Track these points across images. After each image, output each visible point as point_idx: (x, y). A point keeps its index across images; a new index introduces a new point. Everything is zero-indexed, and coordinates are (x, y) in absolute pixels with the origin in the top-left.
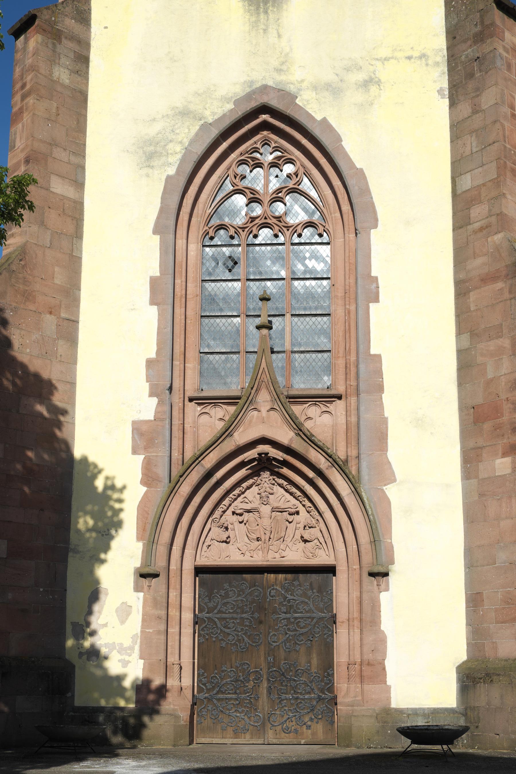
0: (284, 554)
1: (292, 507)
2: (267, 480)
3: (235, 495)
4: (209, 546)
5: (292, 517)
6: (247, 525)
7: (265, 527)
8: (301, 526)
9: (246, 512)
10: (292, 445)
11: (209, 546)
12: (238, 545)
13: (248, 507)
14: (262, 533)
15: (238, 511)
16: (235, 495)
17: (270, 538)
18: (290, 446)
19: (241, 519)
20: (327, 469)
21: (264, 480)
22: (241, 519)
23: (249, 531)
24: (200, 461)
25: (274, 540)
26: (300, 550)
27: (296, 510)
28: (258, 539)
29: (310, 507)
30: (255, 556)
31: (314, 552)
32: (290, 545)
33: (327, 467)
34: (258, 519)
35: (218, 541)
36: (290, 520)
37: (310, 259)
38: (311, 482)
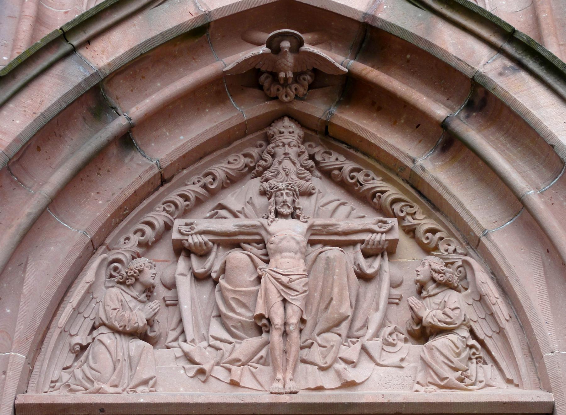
0: (351, 374)
1: (376, 228)
2: (292, 152)
3: (186, 198)
4: (83, 348)
5: (377, 263)
6: (222, 281)
7: (285, 279)
8: (409, 286)
9: (218, 244)
10: (381, 15)
11: (83, 348)
12: (184, 345)
13: (228, 225)
14: (276, 300)
15: (194, 240)
16: (186, 198)
17: (303, 321)
18: (374, 18)
19: (198, 267)
20: (501, 74)
21: (280, 151)
22: (198, 267)
23: (230, 296)
24: (74, 50)
25: (317, 330)
26: (411, 365)
27: (390, 237)
28: (262, 325)
29: (434, 231)
30: (247, 381)
31: (463, 365)
32: (374, 346)
33: (500, 70)
34: (262, 265)
35: (114, 330)
36: (369, 271)
37: (312, 167)
38: (447, 142)
